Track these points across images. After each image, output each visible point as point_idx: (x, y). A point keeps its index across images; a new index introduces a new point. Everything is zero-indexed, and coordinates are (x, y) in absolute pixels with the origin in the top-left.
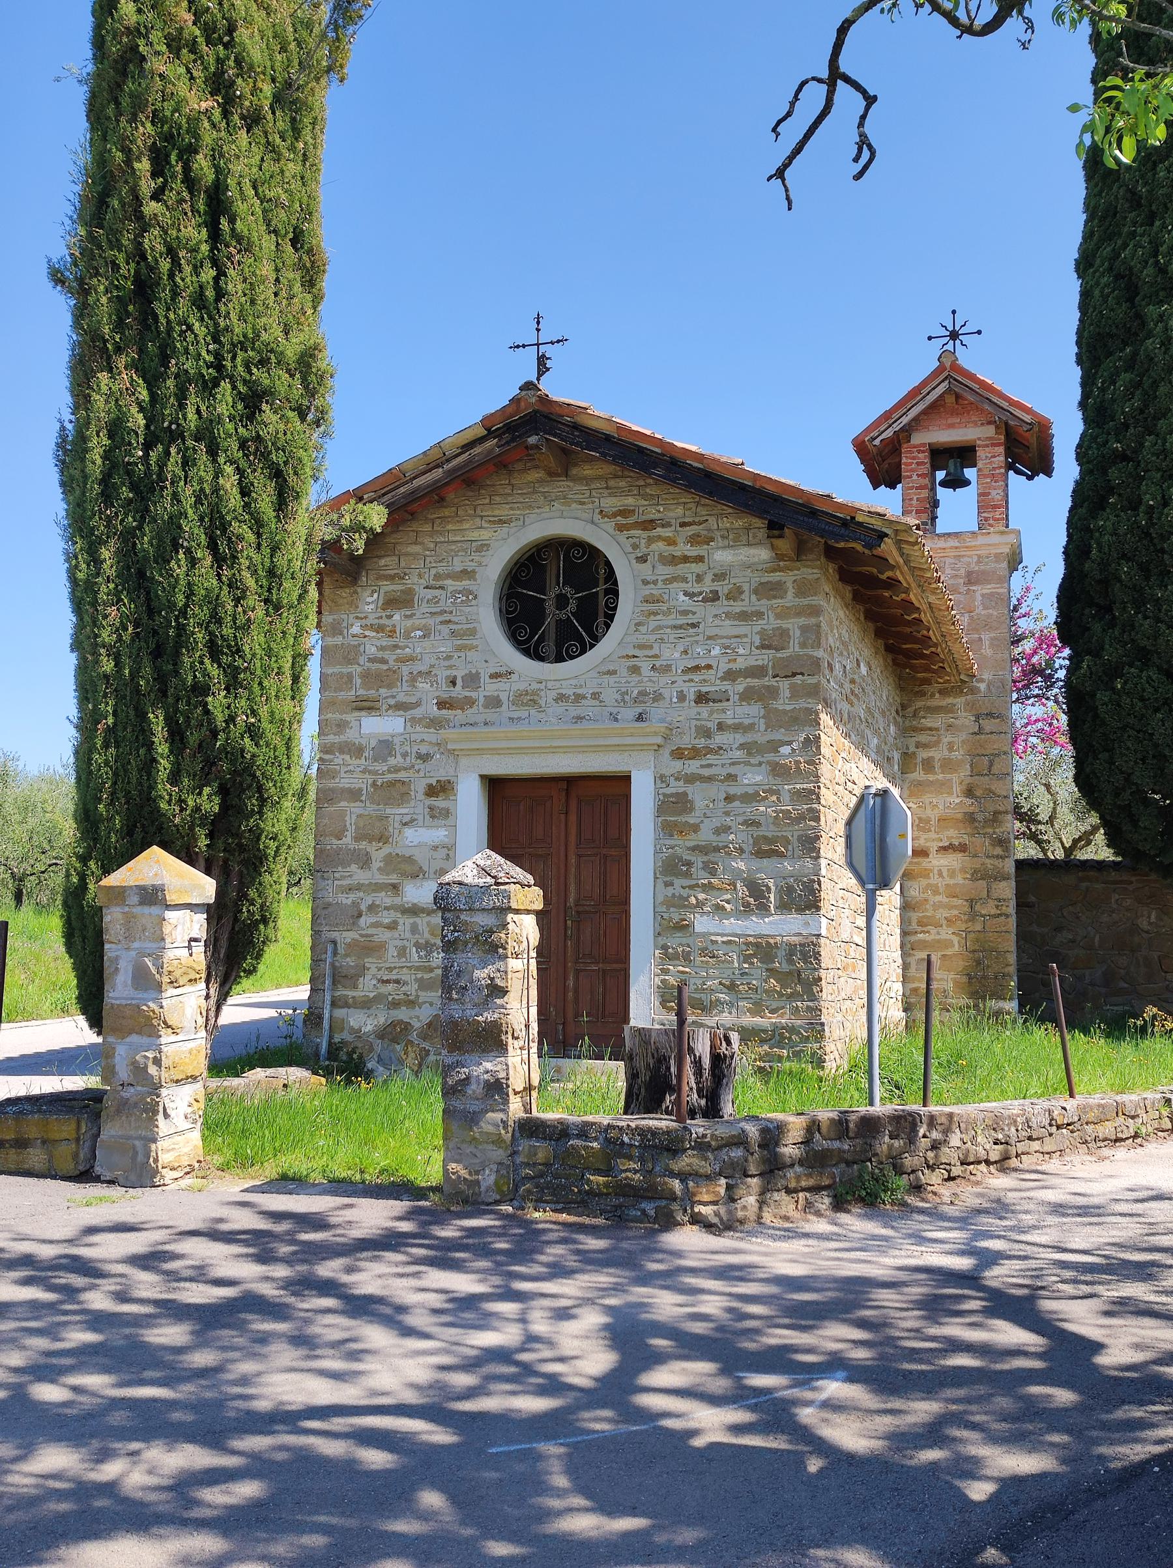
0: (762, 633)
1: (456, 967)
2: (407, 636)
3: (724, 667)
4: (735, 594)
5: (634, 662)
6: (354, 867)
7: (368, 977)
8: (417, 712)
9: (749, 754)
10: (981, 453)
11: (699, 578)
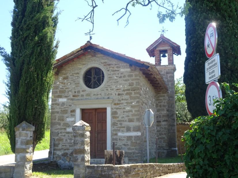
0: (129, 83)
1: (76, 140)
2: (67, 84)
3: (123, 89)
4: (124, 76)
5: (107, 88)
6: (58, 125)
7: (60, 145)
8: (69, 98)
9: (127, 104)
10: (168, 51)
11: (118, 74)
